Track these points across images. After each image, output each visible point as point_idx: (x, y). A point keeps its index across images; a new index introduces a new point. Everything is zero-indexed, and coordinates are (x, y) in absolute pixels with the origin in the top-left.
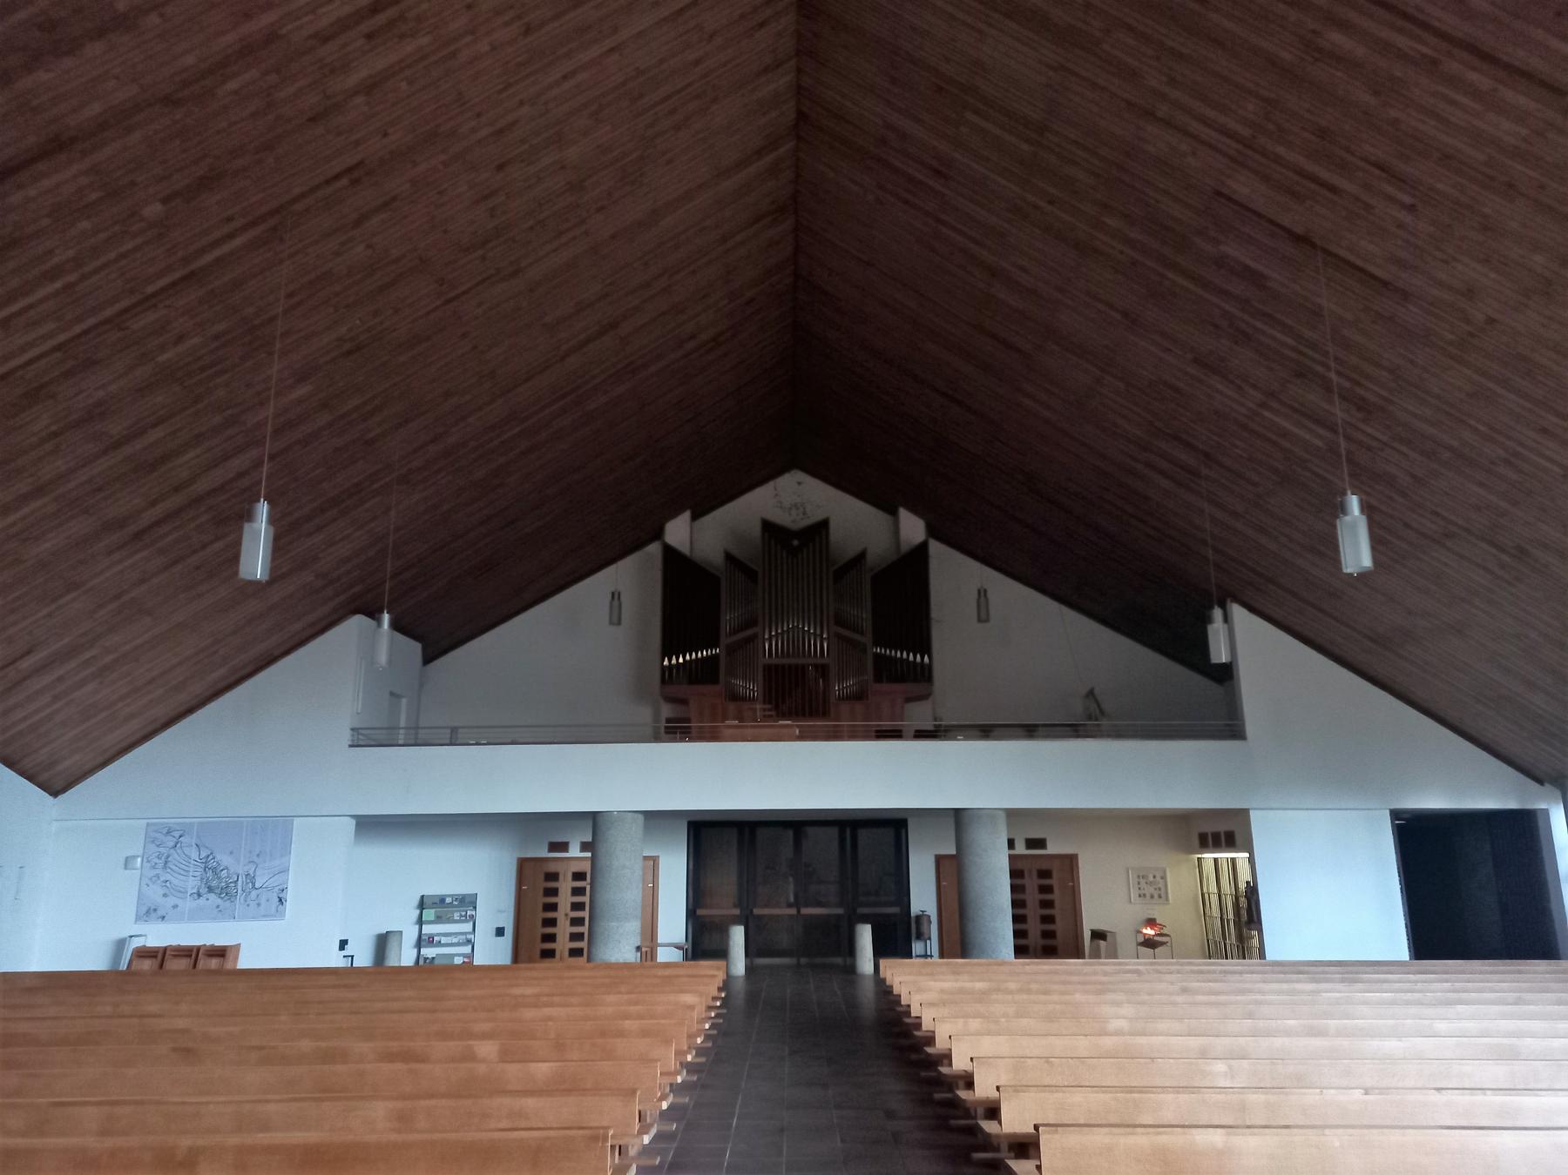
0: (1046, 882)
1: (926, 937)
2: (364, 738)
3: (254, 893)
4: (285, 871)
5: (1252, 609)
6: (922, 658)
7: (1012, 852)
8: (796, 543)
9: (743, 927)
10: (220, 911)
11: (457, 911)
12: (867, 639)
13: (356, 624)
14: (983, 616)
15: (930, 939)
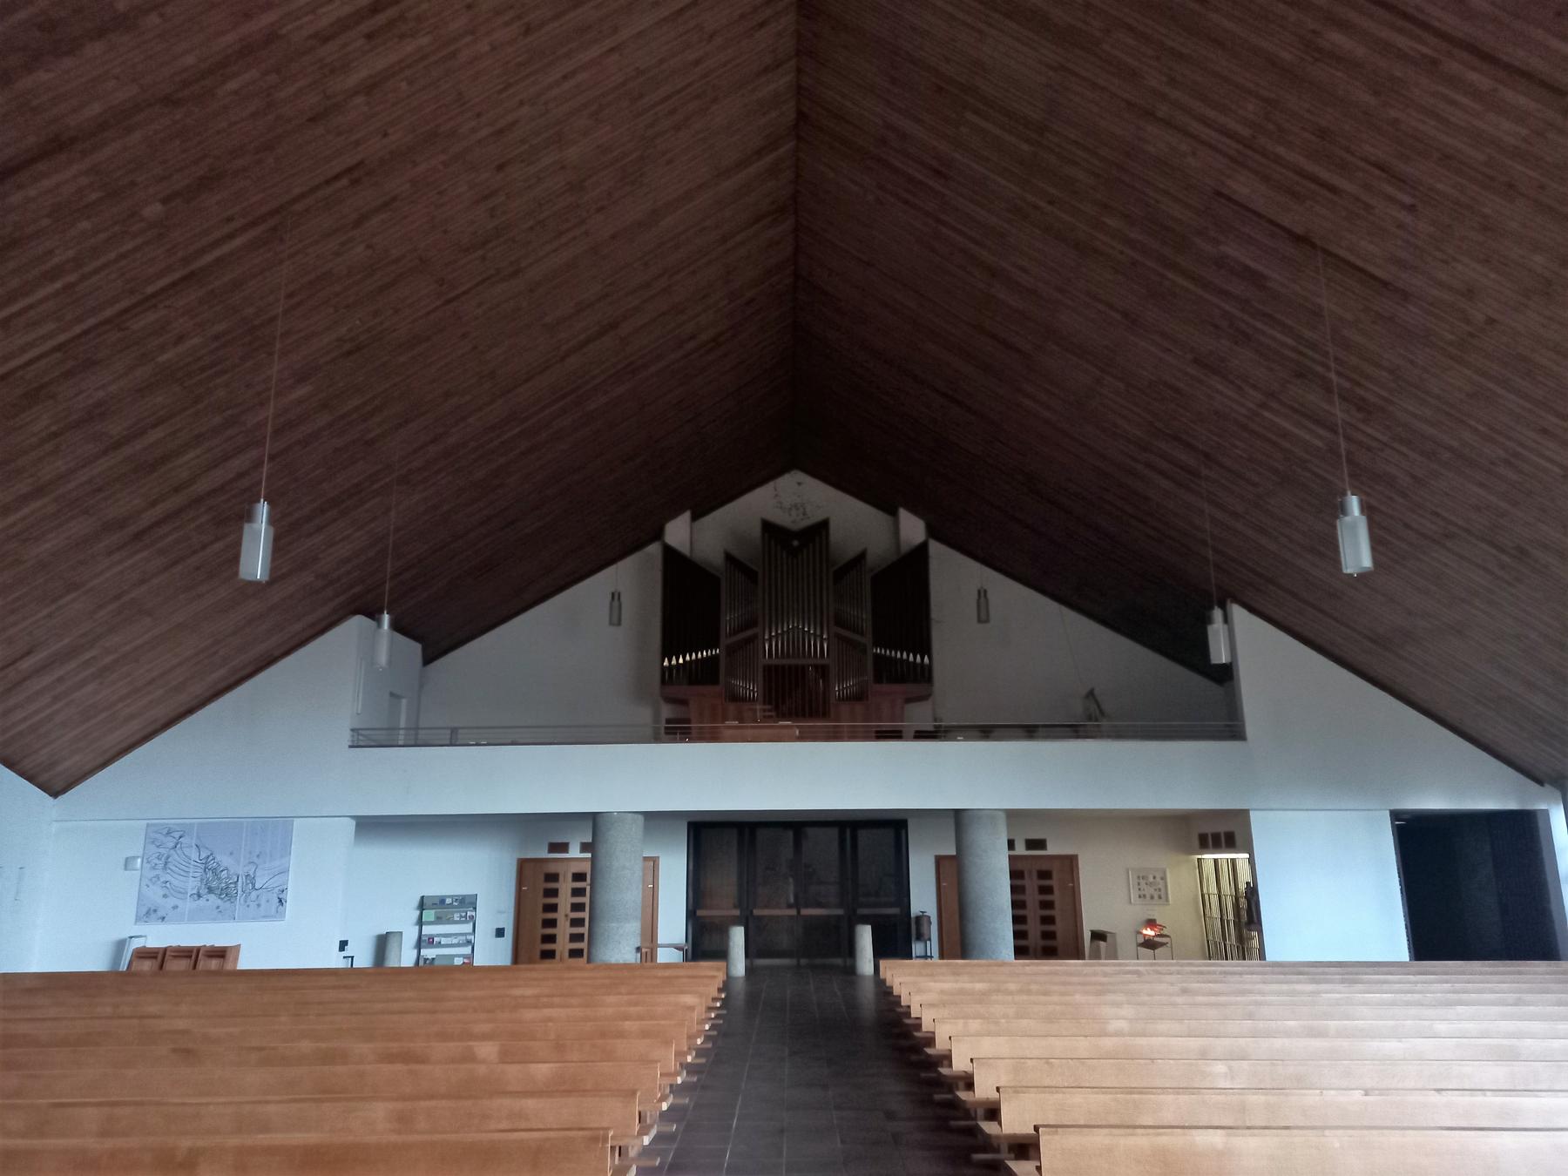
0: (1046, 883)
1: (926, 937)
2: (364, 739)
3: (254, 894)
4: (285, 871)
5: (1252, 610)
6: (922, 659)
7: (1012, 853)
8: (796, 543)
9: (743, 928)
10: (220, 912)
11: (457, 912)
12: (867, 640)
13: (356, 624)
14: (983, 616)
15: (930, 940)
